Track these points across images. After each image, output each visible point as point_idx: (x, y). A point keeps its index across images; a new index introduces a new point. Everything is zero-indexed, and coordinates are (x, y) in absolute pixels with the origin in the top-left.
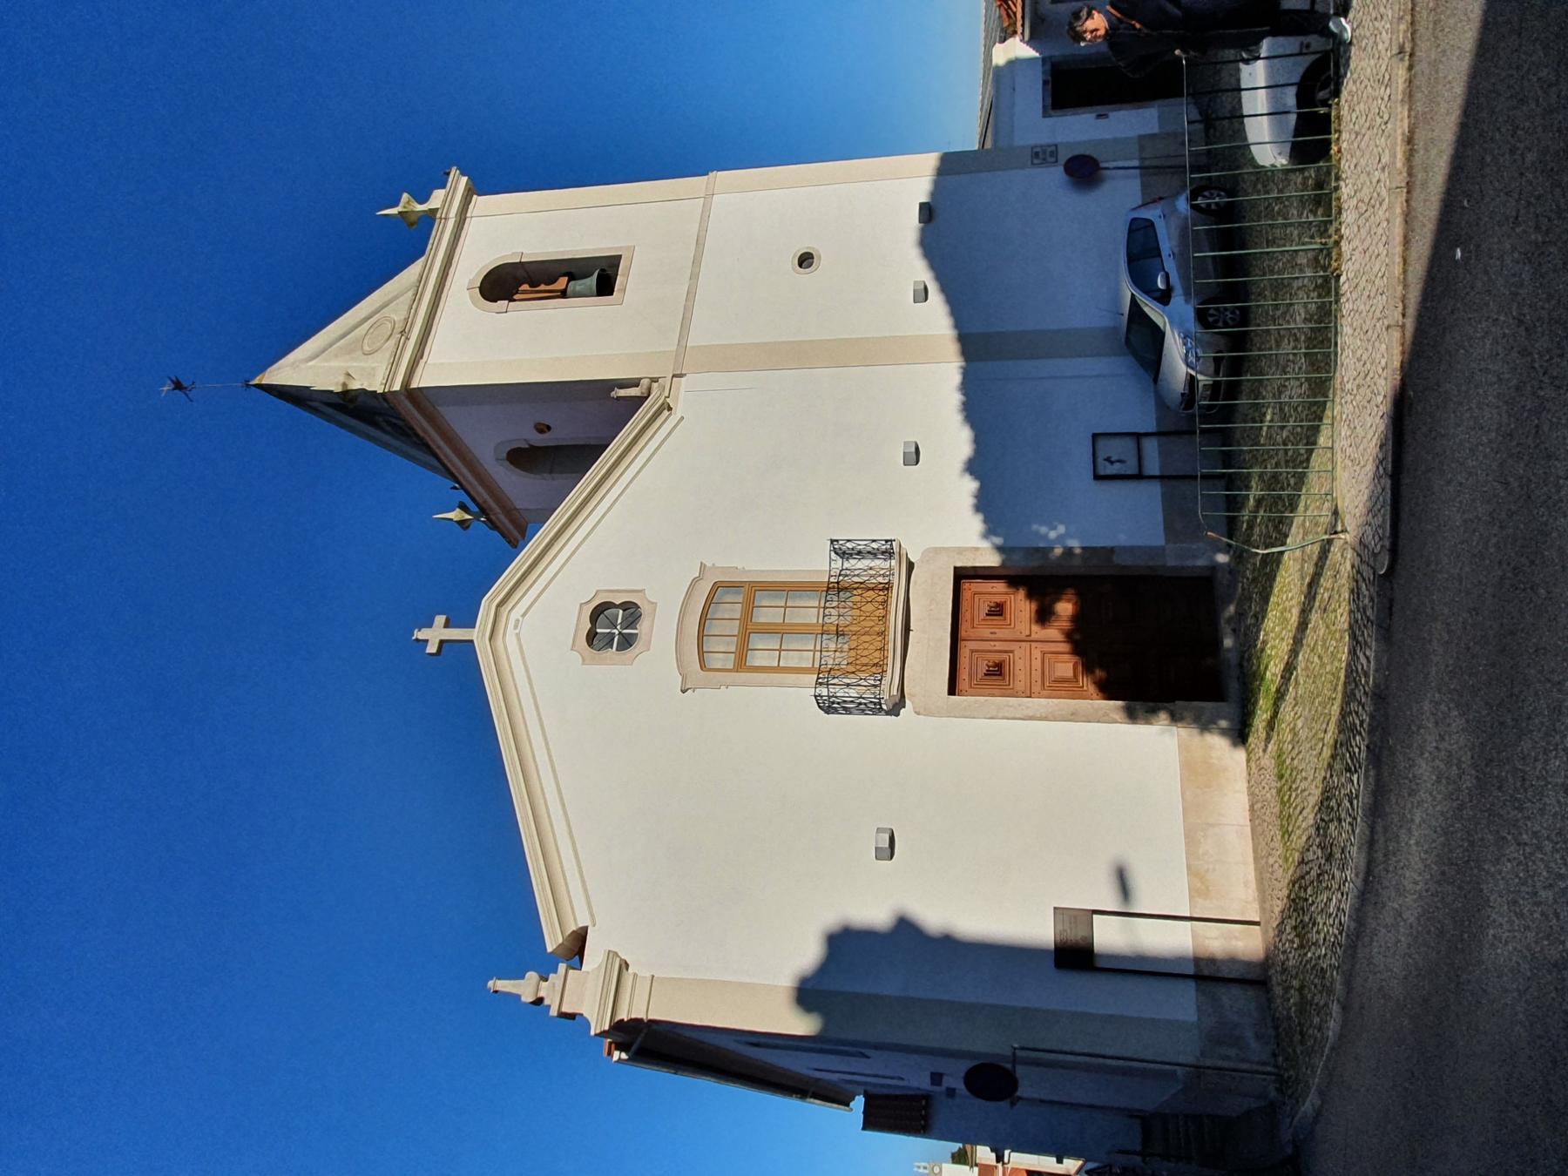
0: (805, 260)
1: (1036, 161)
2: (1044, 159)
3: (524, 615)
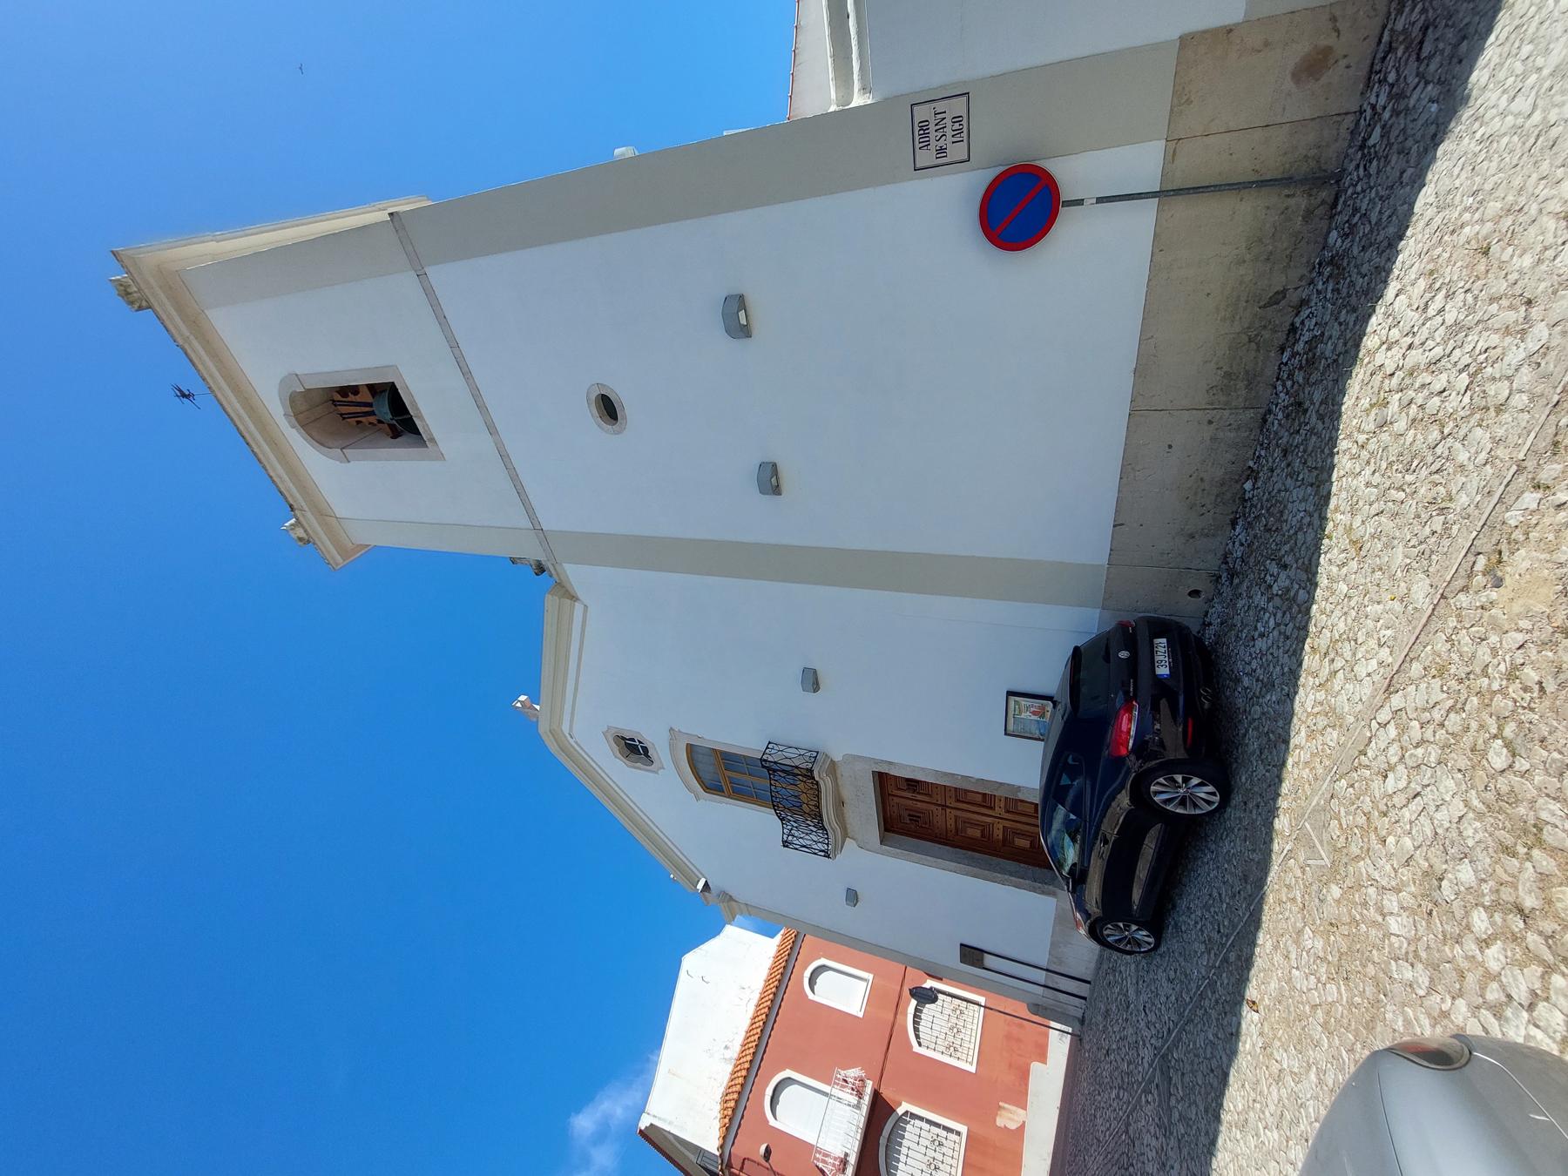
0: (608, 408)
1: (926, 157)
2: (941, 150)
3: (571, 727)
